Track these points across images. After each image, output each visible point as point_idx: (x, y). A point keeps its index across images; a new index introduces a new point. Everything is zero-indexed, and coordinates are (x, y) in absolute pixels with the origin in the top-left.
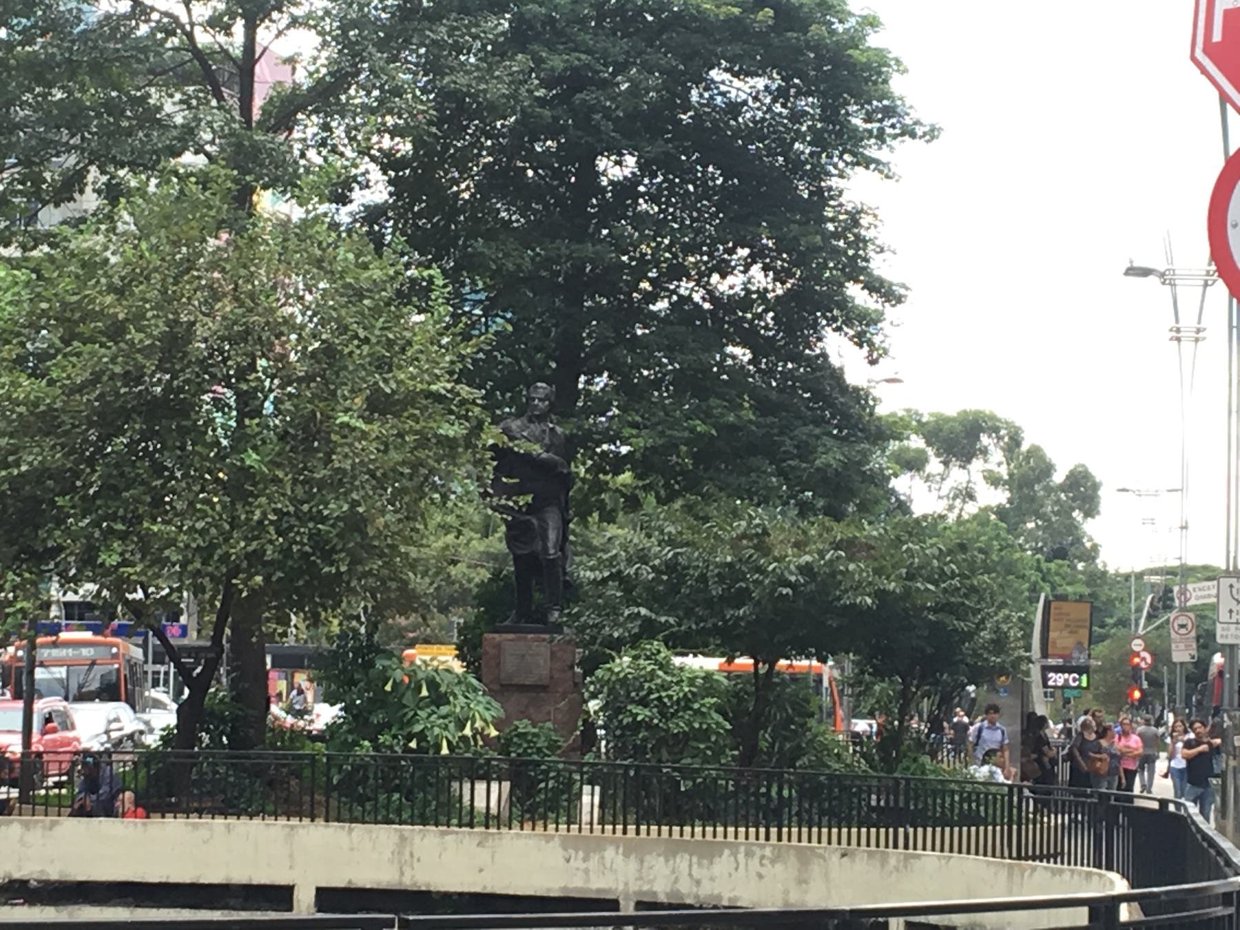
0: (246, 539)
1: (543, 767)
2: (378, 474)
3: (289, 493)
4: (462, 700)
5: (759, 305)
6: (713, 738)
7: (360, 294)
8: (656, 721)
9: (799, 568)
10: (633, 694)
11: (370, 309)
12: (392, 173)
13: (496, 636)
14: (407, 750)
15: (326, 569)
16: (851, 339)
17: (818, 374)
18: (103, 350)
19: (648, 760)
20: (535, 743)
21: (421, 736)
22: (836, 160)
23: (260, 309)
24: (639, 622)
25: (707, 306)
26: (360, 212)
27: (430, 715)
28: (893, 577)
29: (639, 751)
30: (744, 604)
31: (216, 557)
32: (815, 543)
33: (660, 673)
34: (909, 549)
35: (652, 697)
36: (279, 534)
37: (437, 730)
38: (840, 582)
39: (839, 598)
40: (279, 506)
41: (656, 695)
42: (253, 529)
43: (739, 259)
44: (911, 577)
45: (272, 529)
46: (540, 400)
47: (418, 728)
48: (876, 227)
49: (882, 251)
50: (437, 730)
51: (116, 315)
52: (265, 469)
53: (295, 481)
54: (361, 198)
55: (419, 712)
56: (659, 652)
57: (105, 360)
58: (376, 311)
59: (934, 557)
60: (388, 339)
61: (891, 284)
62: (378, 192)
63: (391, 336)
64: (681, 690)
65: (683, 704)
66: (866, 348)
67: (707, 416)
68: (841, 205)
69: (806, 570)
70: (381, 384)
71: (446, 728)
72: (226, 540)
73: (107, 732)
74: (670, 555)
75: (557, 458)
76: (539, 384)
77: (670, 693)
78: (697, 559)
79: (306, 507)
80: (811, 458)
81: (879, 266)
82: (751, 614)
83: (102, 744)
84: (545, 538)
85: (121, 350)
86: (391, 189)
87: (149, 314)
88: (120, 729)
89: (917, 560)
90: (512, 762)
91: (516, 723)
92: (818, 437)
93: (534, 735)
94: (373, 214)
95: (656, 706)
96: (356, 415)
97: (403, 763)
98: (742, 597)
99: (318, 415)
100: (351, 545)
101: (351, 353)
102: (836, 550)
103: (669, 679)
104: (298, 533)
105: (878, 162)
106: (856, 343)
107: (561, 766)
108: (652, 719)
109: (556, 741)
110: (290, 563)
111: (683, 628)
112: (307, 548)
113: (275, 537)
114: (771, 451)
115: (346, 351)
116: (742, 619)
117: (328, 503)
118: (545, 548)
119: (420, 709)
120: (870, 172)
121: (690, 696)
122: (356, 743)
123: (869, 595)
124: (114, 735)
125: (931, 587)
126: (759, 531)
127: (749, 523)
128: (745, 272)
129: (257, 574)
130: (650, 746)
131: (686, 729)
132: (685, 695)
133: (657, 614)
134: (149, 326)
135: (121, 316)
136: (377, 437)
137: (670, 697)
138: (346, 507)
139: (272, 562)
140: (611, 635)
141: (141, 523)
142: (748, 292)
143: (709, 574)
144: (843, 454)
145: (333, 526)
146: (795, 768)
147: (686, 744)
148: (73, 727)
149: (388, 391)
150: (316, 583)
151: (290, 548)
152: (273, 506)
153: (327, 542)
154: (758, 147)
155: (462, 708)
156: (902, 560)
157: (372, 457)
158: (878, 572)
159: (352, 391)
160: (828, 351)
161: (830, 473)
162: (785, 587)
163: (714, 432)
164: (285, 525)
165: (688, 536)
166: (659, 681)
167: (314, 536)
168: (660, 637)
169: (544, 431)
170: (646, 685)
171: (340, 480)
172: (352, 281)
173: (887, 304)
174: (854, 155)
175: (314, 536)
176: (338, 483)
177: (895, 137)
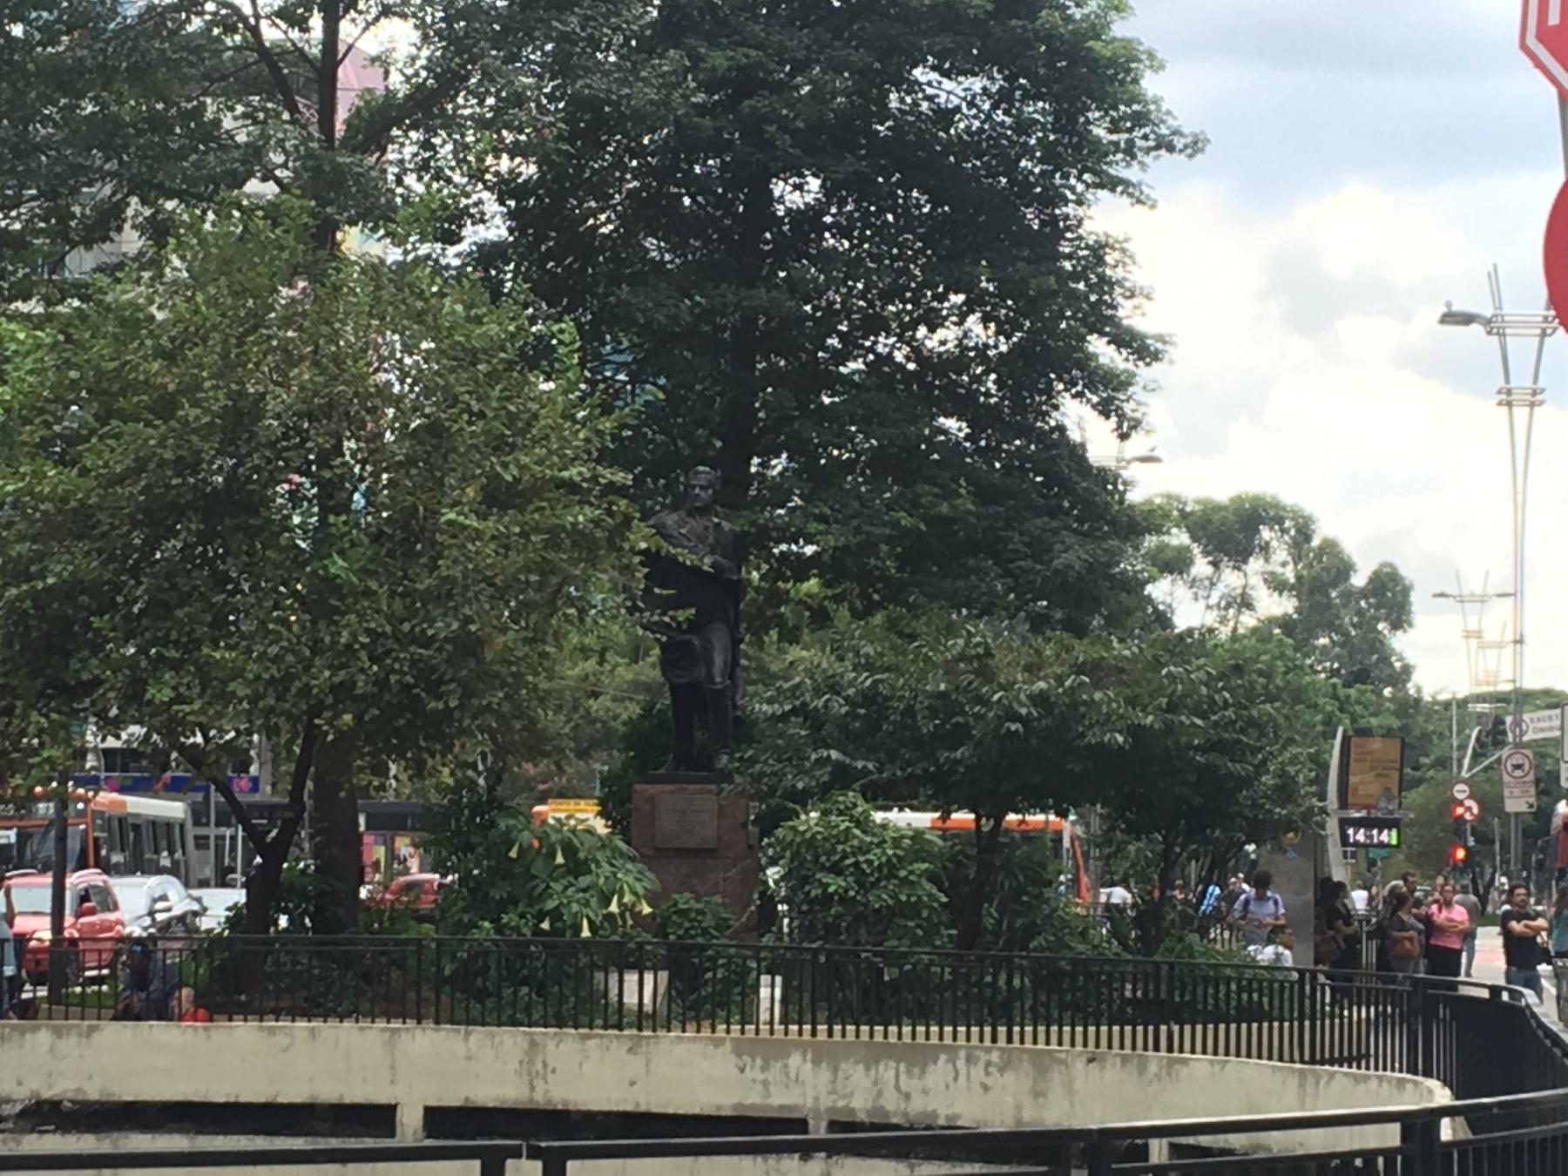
1: (710, 952)
2: (497, 581)
6: (925, 914)
8: (852, 893)
10: (823, 859)
14: (537, 931)
15: (433, 704)
18: (150, 430)
19: (843, 943)
21: (555, 915)
22: (1073, 181)
27: (566, 888)
28: (1150, 709)
29: (832, 931)
31: (293, 691)
33: (857, 832)
34: (1169, 674)
35: (848, 862)
36: (373, 660)
37: (575, 907)
38: (1084, 716)
39: (1083, 735)
40: (373, 625)
42: (340, 655)
43: (952, 307)
45: (363, 655)
46: (702, 488)
47: (551, 904)
50: (575, 907)
51: (164, 386)
53: (392, 594)
54: (473, 235)
56: (855, 805)
57: (152, 442)
58: (492, 377)
59: (1201, 682)
60: (509, 413)
63: (512, 408)
64: (884, 853)
65: (885, 871)
67: (913, 507)
68: (1080, 238)
69: (1039, 700)
70: (498, 469)
71: (587, 904)
72: (307, 669)
73: (151, 913)
75: (724, 561)
76: (701, 468)
77: (870, 857)
78: (902, 688)
79: (406, 627)
81: (1128, 314)
82: (971, 756)
83: (145, 929)
84: (709, 663)
87: (207, 384)
90: (671, 946)
92: (1055, 532)
94: (488, 255)
97: (533, 948)
98: (958, 736)
101: (461, 429)
102: (1078, 674)
103: (868, 839)
104: (396, 659)
105: (1126, 183)
107: (732, 951)
108: (846, 891)
109: (726, 920)
110: (387, 697)
112: (409, 679)
115: (456, 427)
118: (710, 676)
121: (894, 860)
123: (1120, 732)
124: (160, 917)
125: (1199, 722)
126: (981, 650)
128: (959, 324)
129: (345, 712)
131: (890, 902)
132: (889, 860)
133: (853, 758)
134: (207, 399)
135: (171, 387)
137: (869, 862)
138: (455, 626)
139: (364, 697)
141: (199, 649)
143: (918, 706)
146: (1026, 948)
148: (116, 908)
153: (434, 670)
155: (607, 878)
158: (1132, 702)
160: (1067, 422)
162: (1013, 721)
163: (923, 527)
169: (706, 528)
170: (840, 848)
172: (462, 339)
173: (1140, 363)
174: (1095, 173)
176: (444, 595)
177: (1148, 151)
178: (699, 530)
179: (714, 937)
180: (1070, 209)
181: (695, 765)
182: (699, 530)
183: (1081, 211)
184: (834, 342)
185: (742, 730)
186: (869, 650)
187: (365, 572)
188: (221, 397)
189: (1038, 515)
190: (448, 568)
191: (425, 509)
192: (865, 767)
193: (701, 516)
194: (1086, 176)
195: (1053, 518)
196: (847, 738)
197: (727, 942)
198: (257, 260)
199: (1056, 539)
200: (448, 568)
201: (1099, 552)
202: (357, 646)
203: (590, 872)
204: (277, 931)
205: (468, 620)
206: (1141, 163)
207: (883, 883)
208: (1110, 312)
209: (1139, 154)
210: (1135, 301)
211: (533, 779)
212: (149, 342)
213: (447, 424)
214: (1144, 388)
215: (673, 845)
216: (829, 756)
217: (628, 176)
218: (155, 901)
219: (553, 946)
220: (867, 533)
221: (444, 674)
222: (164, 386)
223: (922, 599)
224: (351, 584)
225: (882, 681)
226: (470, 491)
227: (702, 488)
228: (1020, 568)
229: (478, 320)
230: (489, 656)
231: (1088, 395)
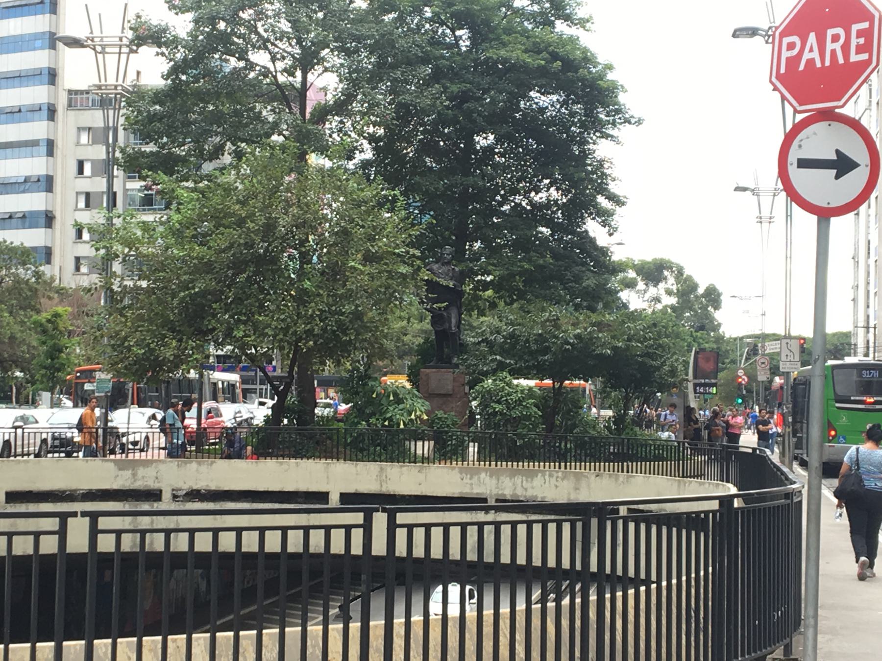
14: (383, 426)
21: (390, 419)
25: (529, 208)
29: (497, 426)
34: (628, 326)
36: (321, 321)
37: (398, 416)
39: (594, 350)
44: (629, 340)
45: (317, 319)
47: (389, 415)
50: (398, 416)
53: (328, 295)
54: (359, 157)
58: (368, 213)
69: (577, 337)
71: (402, 415)
72: (295, 324)
73: (235, 418)
79: (334, 308)
81: (613, 187)
84: (450, 322)
90: (435, 431)
92: (584, 272)
93: (446, 418)
94: (365, 165)
105: (612, 136)
112: (335, 328)
118: (450, 327)
124: (238, 419)
135: (243, 215)
137: (512, 399)
138: (353, 308)
139: (318, 335)
148: (221, 416)
153: (345, 325)
158: (613, 337)
174: (601, 132)
176: (349, 296)
177: (621, 124)
180: (591, 146)
181: (444, 362)
185: (462, 348)
186: (512, 317)
205: (357, 306)
222: (241, 215)
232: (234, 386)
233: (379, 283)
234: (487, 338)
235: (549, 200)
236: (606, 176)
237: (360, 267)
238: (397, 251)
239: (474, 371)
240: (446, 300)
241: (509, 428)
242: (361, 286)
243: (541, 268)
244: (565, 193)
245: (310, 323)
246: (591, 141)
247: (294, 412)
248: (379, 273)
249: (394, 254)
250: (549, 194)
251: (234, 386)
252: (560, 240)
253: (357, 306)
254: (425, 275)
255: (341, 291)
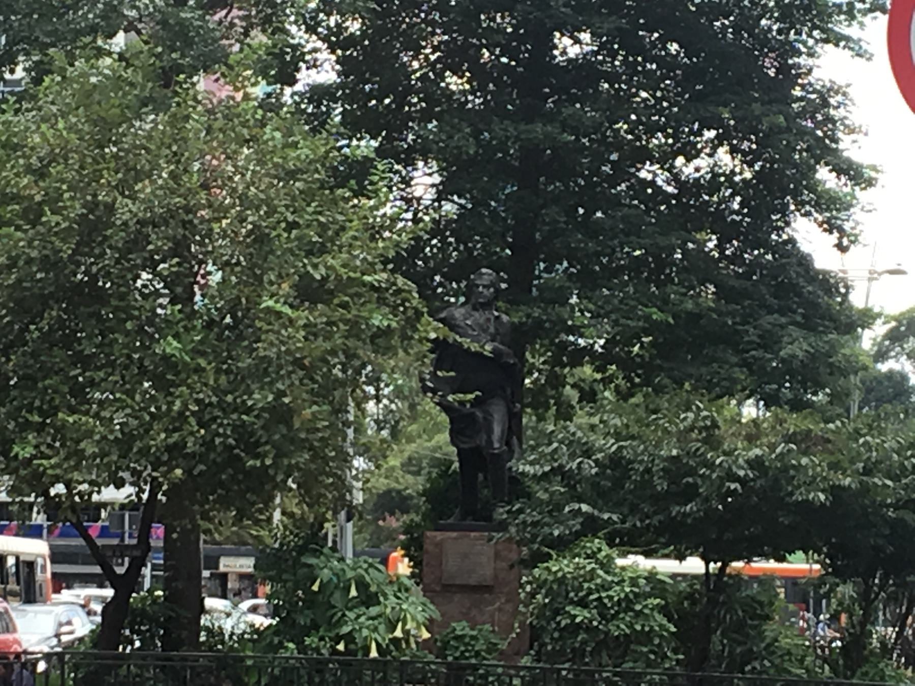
0: (166, 430)
1: (481, 671)
2: (306, 362)
3: (211, 382)
4: (393, 599)
5: (726, 188)
6: (657, 641)
7: (292, 175)
8: (595, 623)
9: (747, 462)
10: (572, 594)
11: (301, 192)
12: (339, 52)
13: (438, 533)
14: (335, 652)
15: (251, 463)
16: (820, 225)
17: (784, 261)
18: (19, 234)
19: (587, 664)
20: (473, 646)
21: (349, 638)
22: (804, 36)
23: (182, 190)
24: (581, 520)
25: (670, 189)
26: (306, 92)
27: (359, 616)
28: (849, 472)
29: (578, 654)
30: (691, 501)
31: (135, 450)
32: (767, 435)
33: (600, 572)
34: (866, 443)
35: (592, 597)
36: (201, 425)
37: (365, 632)
38: (793, 477)
39: (791, 494)
40: (201, 396)
41: (595, 596)
42: (174, 420)
43: (706, 142)
44: (867, 472)
45: (192, 421)
46: (484, 286)
47: (346, 629)
48: (845, 105)
49: (852, 131)
50: (365, 632)
51: (32, 197)
52: (187, 359)
53: (218, 371)
54: (306, 78)
55: (347, 613)
56: (600, 550)
57: (21, 244)
58: (308, 195)
59: (893, 450)
60: (320, 223)
61: (862, 166)
62: (325, 72)
63: (322, 219)
64: (623, 590)
65: (624, 605)
66: (836, 234)
67: (664, 304)
68: (810, 84)
69: (756, 464)
70: (309, 268)
71: (375, 629)
72: (147, 431)
73: (57, 636)
74: (614, 448)
75: (501, 347)
76: (484, 270)
77: (611, 593)
78: (642, 453)
79: (229, 398)
80: (776, 348)
81: (850, 148)
82: (699, 510)
83: (52, 648)
84: (490, 432)
85: (38, 233)
86: (338, 67)
87: (66, 195)
88: (71, 633)
89: (874, 454)
90: (449, 665)
91: (454, 624)
92: (782, 327)
93: (473, 638)
94: (318, 93)
95: (595, 607)
96: (282, 300)
97: (331, 666)
98: (690, 493)
99: (244, 300)
100: (277, 437)
101: (279, 236)
102: (787, 443)
103: (609, 578)
104: (221, 425)
105: (848, 39)
106: (825, 230)
107: (500, 670)
108: (591, 622)
109: (496, 644)
110: (212, 456)
111: (627, 525)
112: (231, 441)
113: (196, 428)
114: (732, 339)
115: (274, 233)
116: (689, 515)
117: (253, 393)
118: (490, 442)
119: (350, 609)
120: (840, 49)
121: (631, 596)
122: (281, 645)
123: (823, 491)
124: (65, 638)
125: (889, 483)
126: (708, 423)
127: (697, 415)
128: (711, 155)
129: (177, 467)
130: (589, 649)
131: (628, 631)
132: (627, 595)
133: (600, 511)
134: (65, 208)
135: (38, 198)
136: (305, 326)
137: (611, 598)
138: (270, 398)
139: (193, 455)
140: (551, 534)
141: (56, 414)
142: (715, 176)
143: (654, 469)
144: (810, 345)
145: (257, 417)
146: (743, 672)
147: (628, 647)
148: (15, 630)
149: (318, 277)
150: (241, 477)
151: (213, 441)
152: (195, 396)
153: (252, 434)
154: (723, 24)
155: (393, 608)
156: (859, 454)
157: (299, 345)
158: (834, 466)
159: (280, 276)
160: (796, 236)
161: (796, 364)
162: (734, 482)
163: (671, 321)
164: (207, 417)
165: (634, 430)
166: (599, 581)
167: (240, 429)
168: (600, 534)
169: (488, 320)
170: (586, 585)
171: (266, 369)
172: (280, 161)
173: (857, 188)
174: (823, 31)
175: (240, 429)
176: (263, 371)
177: (865, 13)
178: (482, 321)
179: (485, 659)
180: (802, 60)
181: (478, 516)
182: (482, 321)
183: (810, 62)
184: (606, 169)
185: (516, 488)
186: (618, 421)
187: (197, 352)
188: (78, 206)
189: (771, 312)
190: (265, 349)
191: (247, 299)
192: (610, 518)
193: (484, 310)
194: (816, 33)
195: (782, 315)
196: (599, 495)
197: (495, 662)
198: (112, 94)
199: (784, 333)
200: (265, 349)
201: (821, 344)
202: (188, 413)
203: (379, 603)
204: (132, 649)
205: (281, 394)
206: (861, 24)
207: (621, 616)
208: (834, 146)
209: (858, 16)
210: (853, 137)
211: (394, 530)
212: (21, 161)
213: (267, 231)
214: (862, 209)
215: (458, 582)
216: (580, 509)
217: (438, 31)
218: (61, 625)
219: (349, 664)
220: (622, 325)
221: (261, 437)
222: (32, 197)
223: (667, 381)
224: (185, 364)
225: (625, 447)
226: (285, 286)
227: (484, 286)
228: (753, 357)
229: (295, 145)
230: (297, 425)
231: (816, 215)
232: (31, 565)
233: (328, 346)
234: (561, 466)
235: (715, 176)
236: (834, 122)
237: (287, 310)
238: (367, 278)
239: (534, 536)
240: (484, 389)
241: (605, 659)
242: (288, 352)
243: (695, 317)
244: (749, 159)
245: (175, 430)
246: (804, 50)
247: (152, 620)
248: (328, 323)
249: (364, 284)
250: (716, 159)
251: (31, 565)
252: (736, 259)
253: (281, 394)
254: (432, 330)
255: (246, 362)
